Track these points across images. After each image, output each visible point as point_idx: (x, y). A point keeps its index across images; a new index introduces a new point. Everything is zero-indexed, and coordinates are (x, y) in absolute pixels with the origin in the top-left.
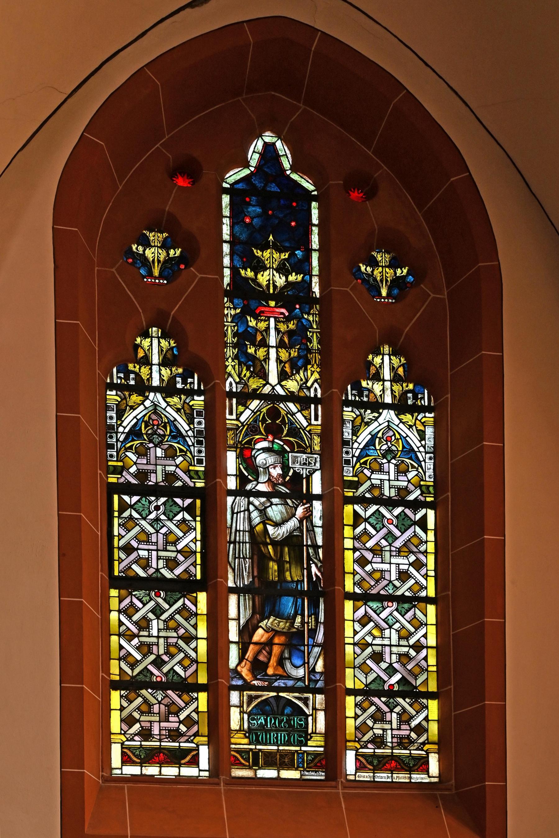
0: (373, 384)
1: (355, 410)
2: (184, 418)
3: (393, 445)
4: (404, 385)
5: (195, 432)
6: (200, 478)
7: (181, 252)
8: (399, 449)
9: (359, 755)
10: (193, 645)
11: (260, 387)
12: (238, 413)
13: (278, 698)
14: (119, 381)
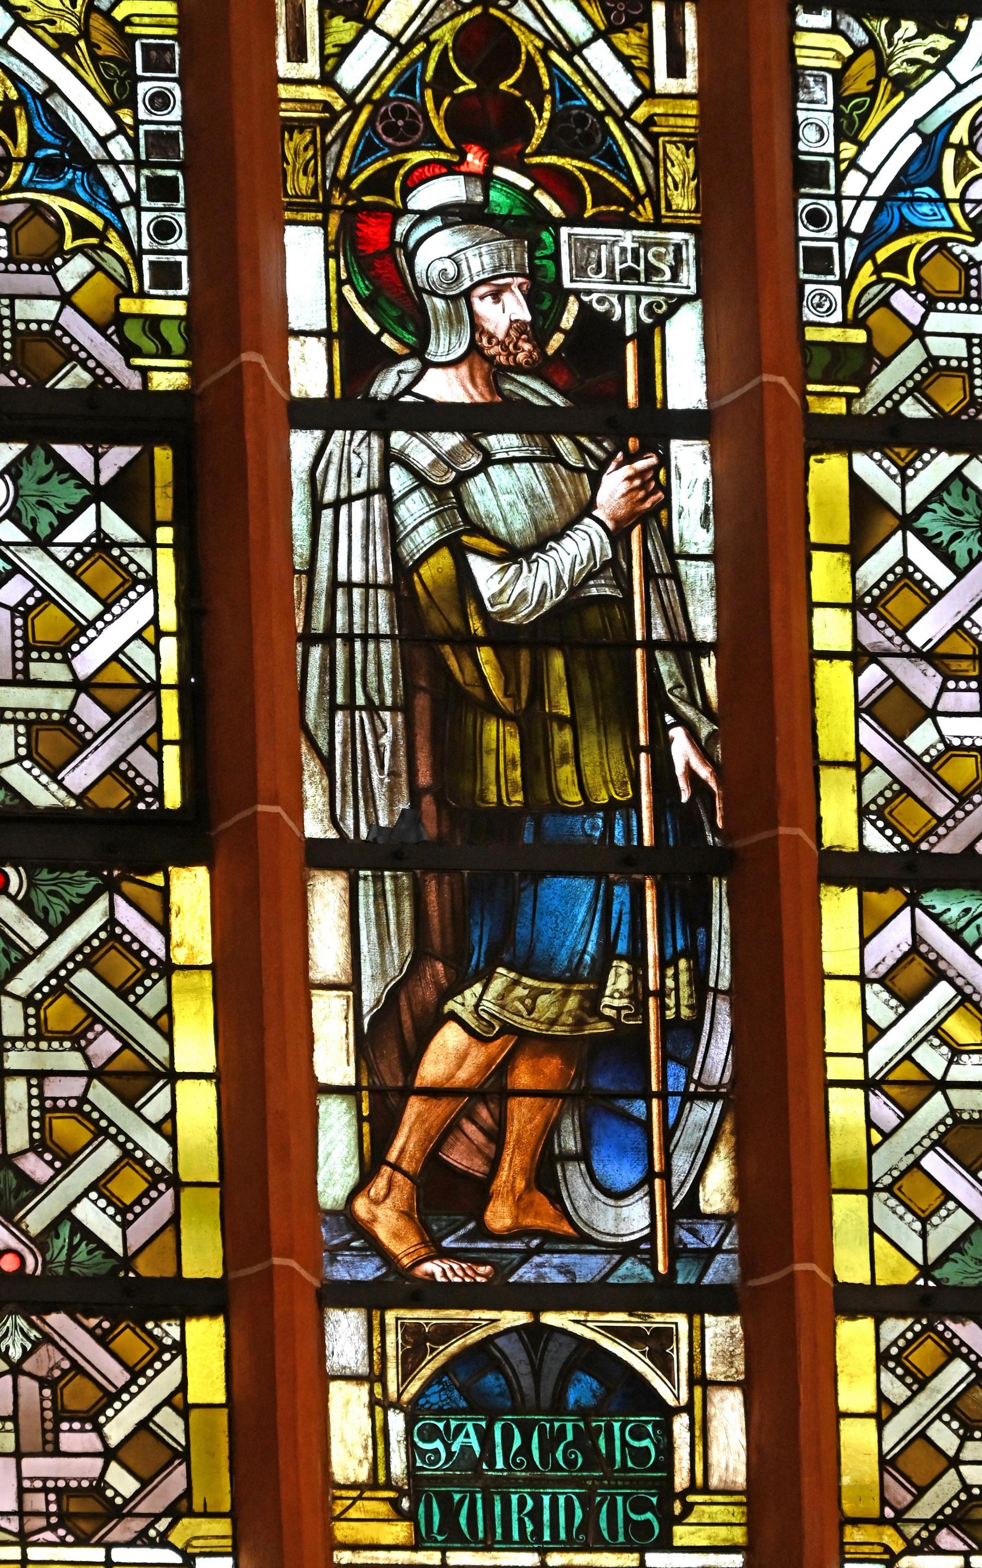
1: (847, 22)
5: (142, 142)
12: (330, 50)
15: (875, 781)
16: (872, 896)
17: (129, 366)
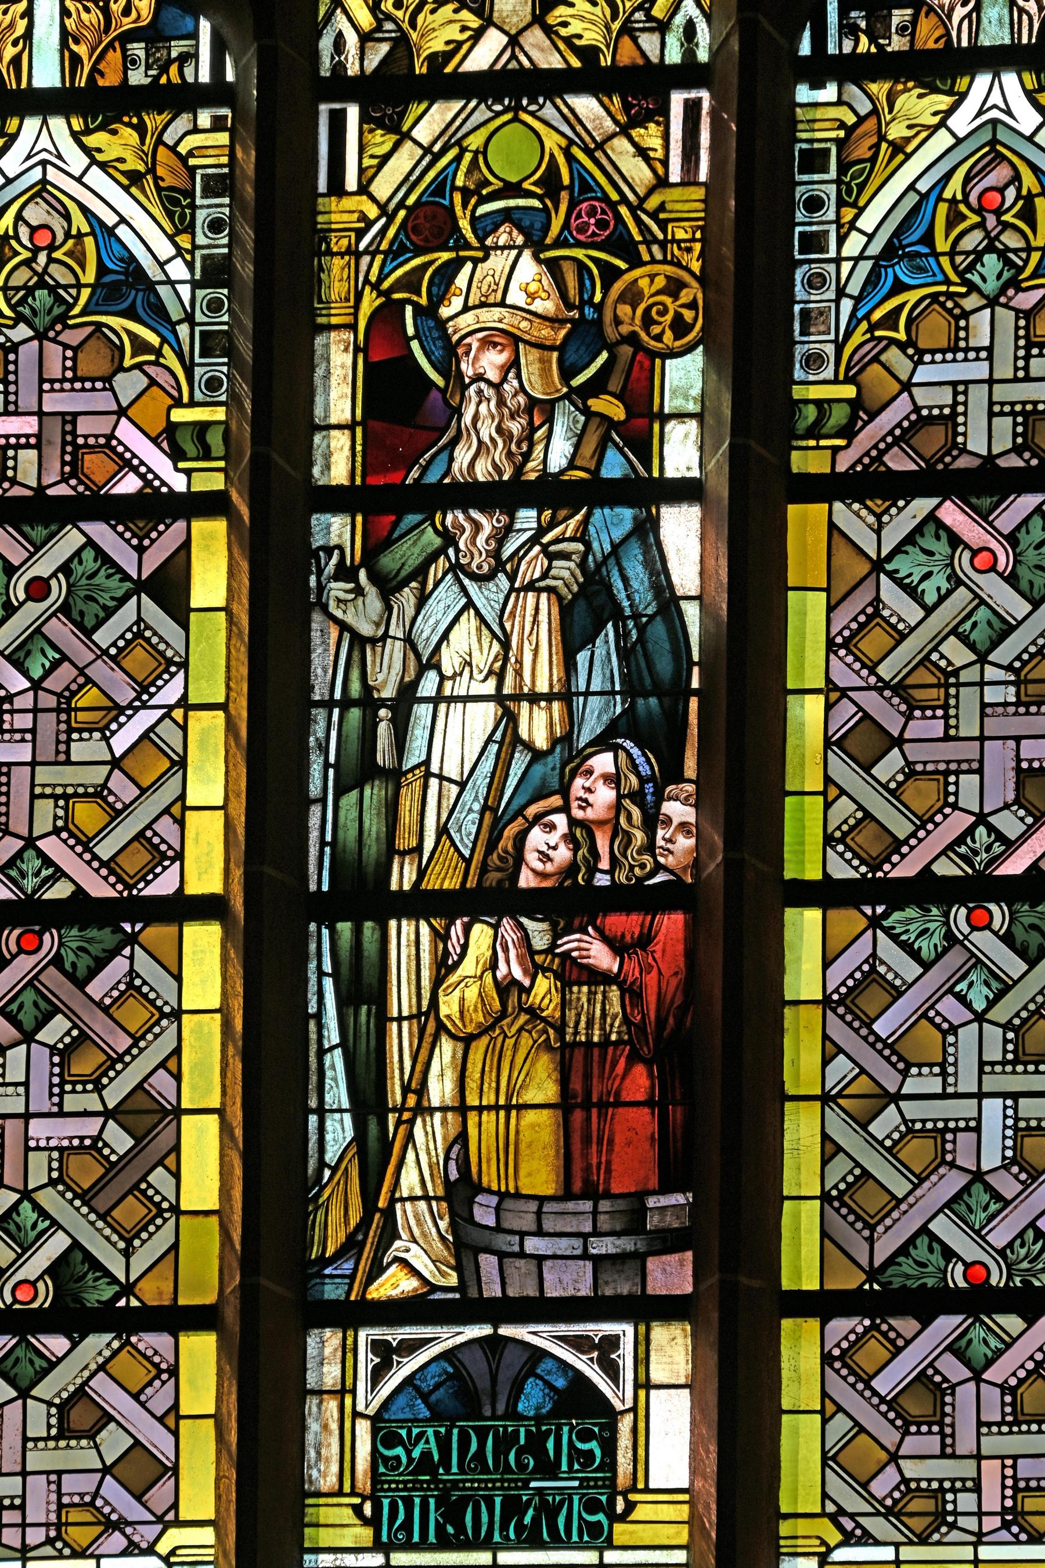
1: (853, 91)
2: (157, 212)
3: (1006, 226)
5: (198, 265)
8: (84, 280)
11: (460, 44)
13: (494, 1344)
14: (848, 47)
15: (844, 807)
17: (177, 470)
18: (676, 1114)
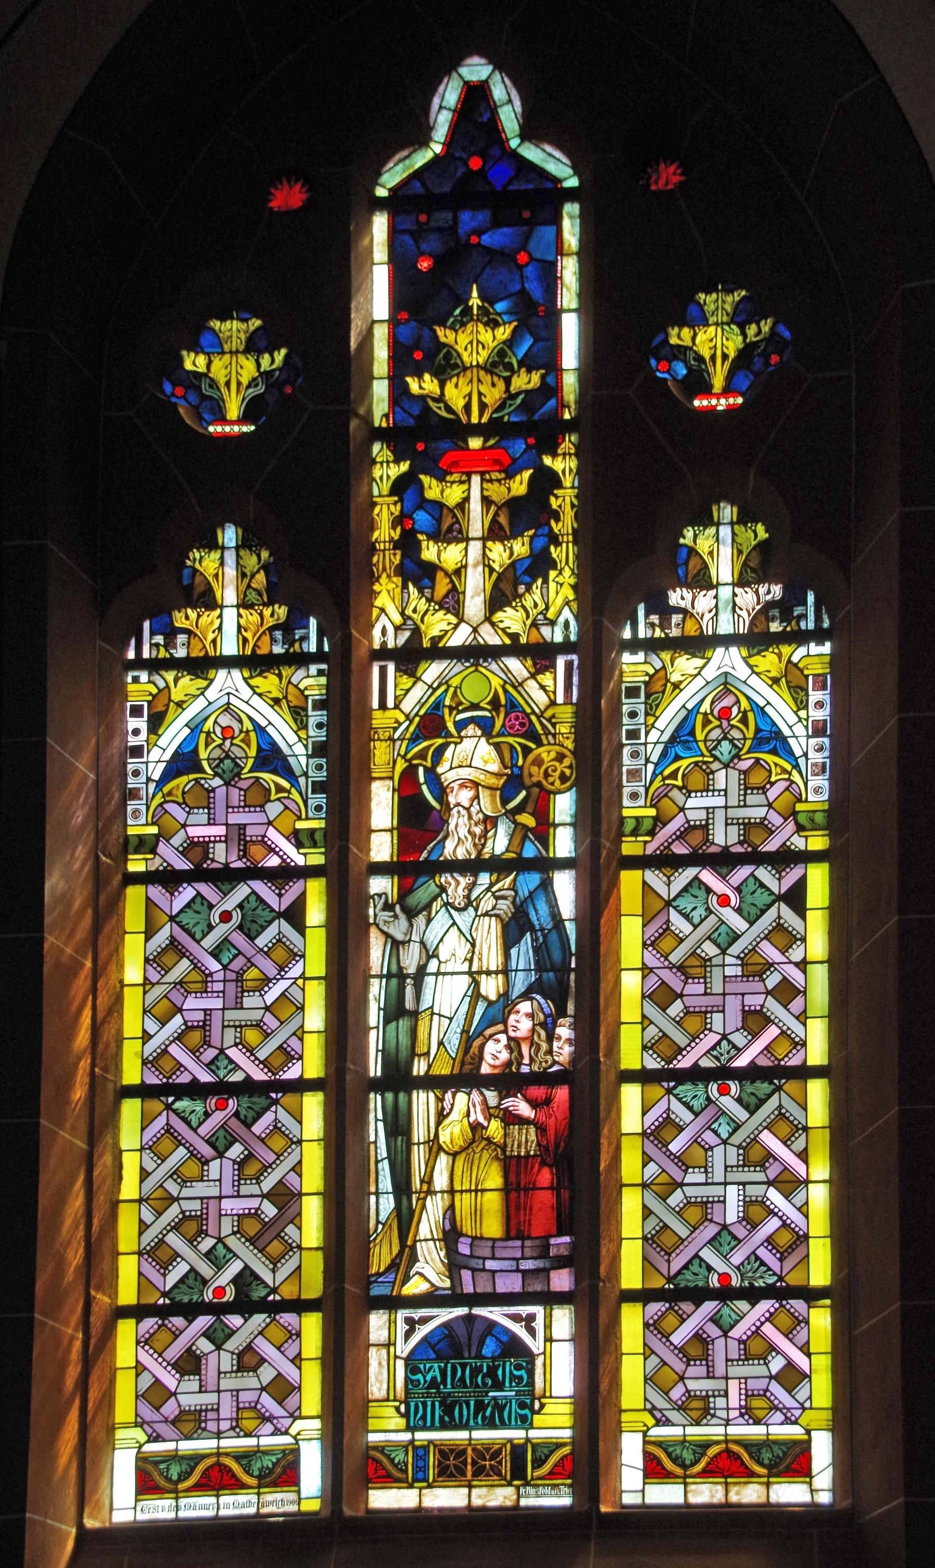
0: (199, 616)
3: (733, 726)
4: (762, 590)
6: (315, 845)
7: (287, 357)
9: (650, 1443)
10: (799, 1199)
11: (447, 632)
12: (398, 693)
13: (469, 1319)
15: (652, 1031)
16: (648, 1088)
18: (565, 1194)
